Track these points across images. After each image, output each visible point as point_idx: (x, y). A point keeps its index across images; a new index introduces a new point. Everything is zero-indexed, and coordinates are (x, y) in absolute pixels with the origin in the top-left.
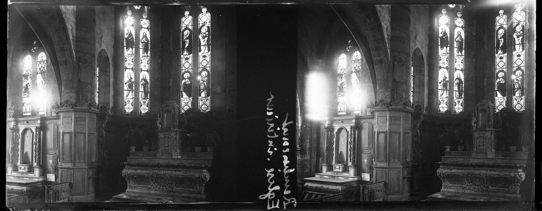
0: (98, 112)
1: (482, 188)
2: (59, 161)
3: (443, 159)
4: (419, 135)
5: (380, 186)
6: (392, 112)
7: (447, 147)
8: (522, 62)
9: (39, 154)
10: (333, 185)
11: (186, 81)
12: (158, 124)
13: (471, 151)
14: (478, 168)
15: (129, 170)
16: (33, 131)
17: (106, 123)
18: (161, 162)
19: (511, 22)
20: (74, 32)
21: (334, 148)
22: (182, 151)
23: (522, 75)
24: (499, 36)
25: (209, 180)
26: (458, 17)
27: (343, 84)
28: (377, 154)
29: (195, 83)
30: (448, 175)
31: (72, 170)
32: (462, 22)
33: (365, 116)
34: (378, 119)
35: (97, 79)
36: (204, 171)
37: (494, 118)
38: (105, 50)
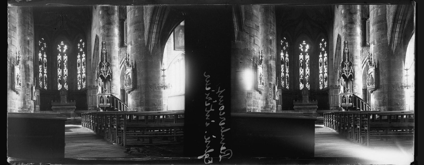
24: (301, 62)
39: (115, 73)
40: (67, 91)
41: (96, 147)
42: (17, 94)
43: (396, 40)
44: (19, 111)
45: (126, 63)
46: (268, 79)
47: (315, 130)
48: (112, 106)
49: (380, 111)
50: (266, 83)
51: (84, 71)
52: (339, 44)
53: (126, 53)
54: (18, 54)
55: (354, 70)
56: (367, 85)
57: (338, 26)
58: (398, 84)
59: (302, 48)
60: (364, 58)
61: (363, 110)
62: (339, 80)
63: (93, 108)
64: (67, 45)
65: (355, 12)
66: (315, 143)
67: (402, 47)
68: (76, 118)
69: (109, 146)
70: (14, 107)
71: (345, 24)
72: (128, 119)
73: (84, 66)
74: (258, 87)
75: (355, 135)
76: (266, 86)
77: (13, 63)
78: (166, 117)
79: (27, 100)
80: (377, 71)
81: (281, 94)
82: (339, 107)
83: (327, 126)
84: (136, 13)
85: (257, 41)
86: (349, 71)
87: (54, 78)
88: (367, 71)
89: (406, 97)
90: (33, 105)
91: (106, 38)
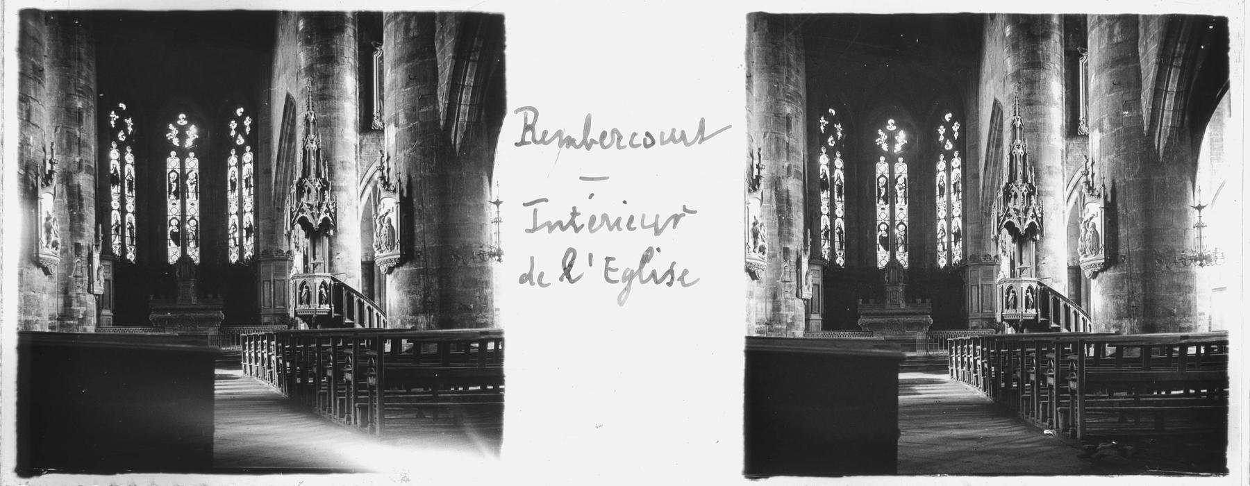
11: (173, 228)
12: (177, 274)
23: (905, 230)
24: (880, 185)
30: (871, 323)
39: (1051, 217)
40: (904, 273)
41: (992, 443)
42: (753, 279)
43: (464, 114)
44: (757, 332)
45: (1084, 186)
46: (70, 230)
47: (216, 387)
48: (1042, 316)
49: (1119, 334)
50: (63, 244)
51: (957, 211)
52: (288, 123)
53: (1086, 156)
54: (756, 156)
55: (1041, 208)
56: (375, 249)
57: (285, 69)
58: (471, 247)
59: (178, 136)
60: (1071, 172)
61: (363, 325)
62: (289, 235)
63: (277, 320)
64: (904, 130)
65: (1046, 32)
66: (216, 427)
67: (1188, 138)
68: (931, 353)
69: (1034, 439)
70: (37, 315)
71: (309, 63)
72: (1091, 357)
73: (958, 194)
74: (40, 256)
75: (338, 402)
76: (64, 252)
77: (34, 181)
78: (1205, 349)
79: (783, 299)
80: (406, 206)
81: (109, 276)
82: (289, 316)
83: (960, 378)
84: (1115, 32)
85: (38, 115)
86: (1026, 211)
88: (376, 206)
89: (494, 286)
90: (95, 309)
91: (319, 105)
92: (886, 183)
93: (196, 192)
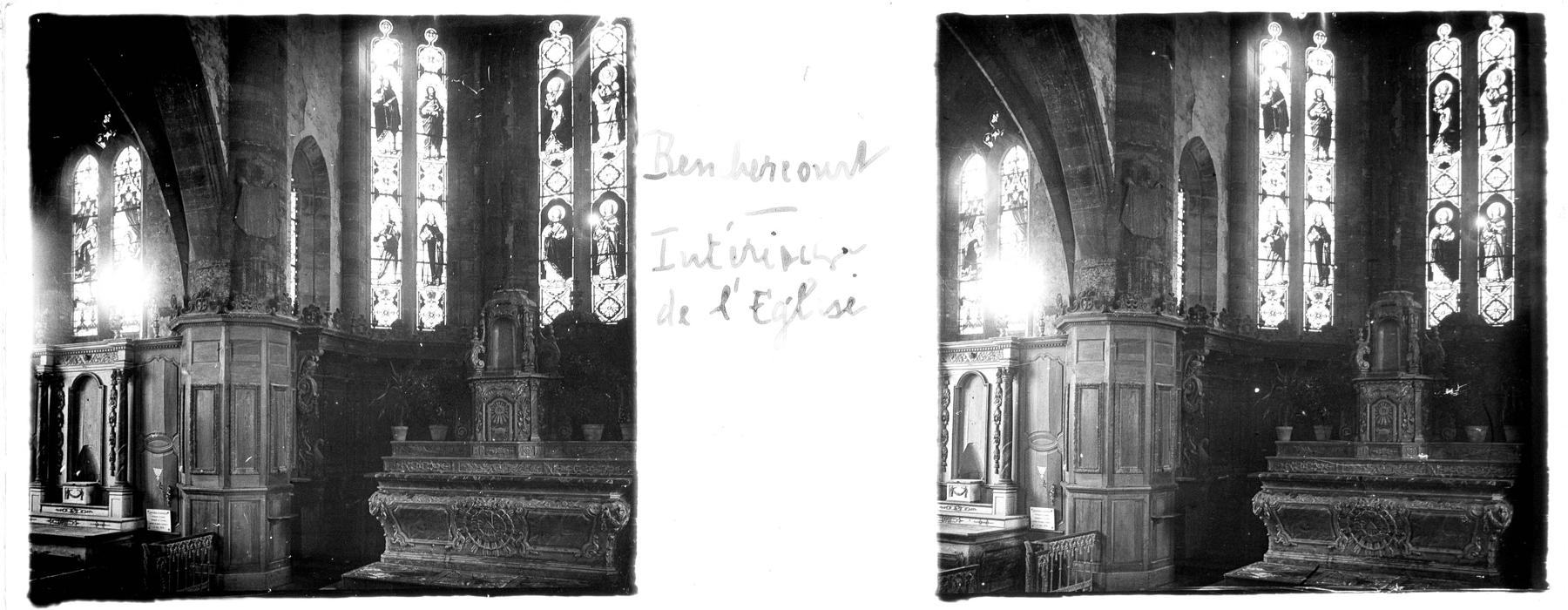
0: (298, 326)
1: (1384, 549)
2: (184, 472)
3: (1270, 463)
4: (315, 394)
5: (202, 546)
6: (1118, 328)
7: (399, 428)
8: (619, 174)
9: (123, 452)
10: (958, 544)
11: (1441, 231)
12: (1359, 360)
13: (470, 440)
14: (490, 491)
15: (1272, 494)
16: (990, 382)
17: (320, 357)
18: (1369, 471)
19: (583, 57)
20: (1110, 88)
21: (947, 434)
22: (1430, 441)
23: (1508, 217)
25: (1510, 524)
26: (426, 43)
27: (89, 246)
28: (192, 451)
29: (581, 236)
31: (1106, 497)
32: (440, 57)
33: (155, 341)
34: (193, 349)
35: (1177, 225)
36: (1497, 497)
37: (538, 340)
38: (313, 138)
87: (504, 233)
92: (1455, 95)
93: (1508, 124)
